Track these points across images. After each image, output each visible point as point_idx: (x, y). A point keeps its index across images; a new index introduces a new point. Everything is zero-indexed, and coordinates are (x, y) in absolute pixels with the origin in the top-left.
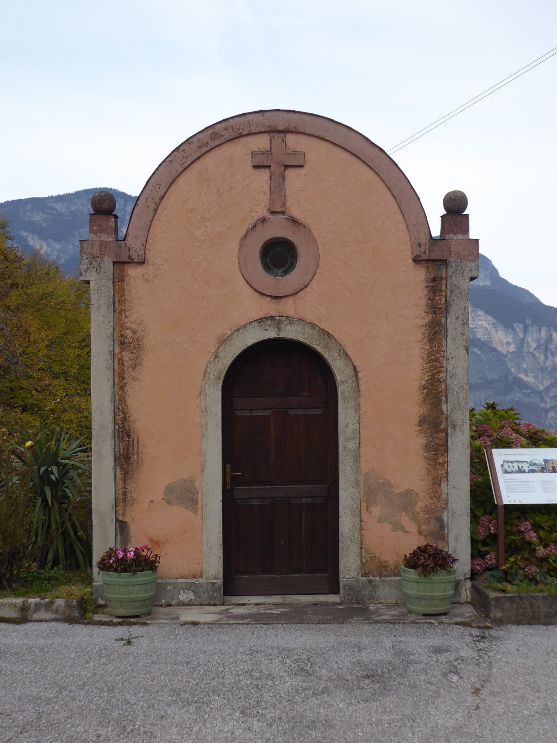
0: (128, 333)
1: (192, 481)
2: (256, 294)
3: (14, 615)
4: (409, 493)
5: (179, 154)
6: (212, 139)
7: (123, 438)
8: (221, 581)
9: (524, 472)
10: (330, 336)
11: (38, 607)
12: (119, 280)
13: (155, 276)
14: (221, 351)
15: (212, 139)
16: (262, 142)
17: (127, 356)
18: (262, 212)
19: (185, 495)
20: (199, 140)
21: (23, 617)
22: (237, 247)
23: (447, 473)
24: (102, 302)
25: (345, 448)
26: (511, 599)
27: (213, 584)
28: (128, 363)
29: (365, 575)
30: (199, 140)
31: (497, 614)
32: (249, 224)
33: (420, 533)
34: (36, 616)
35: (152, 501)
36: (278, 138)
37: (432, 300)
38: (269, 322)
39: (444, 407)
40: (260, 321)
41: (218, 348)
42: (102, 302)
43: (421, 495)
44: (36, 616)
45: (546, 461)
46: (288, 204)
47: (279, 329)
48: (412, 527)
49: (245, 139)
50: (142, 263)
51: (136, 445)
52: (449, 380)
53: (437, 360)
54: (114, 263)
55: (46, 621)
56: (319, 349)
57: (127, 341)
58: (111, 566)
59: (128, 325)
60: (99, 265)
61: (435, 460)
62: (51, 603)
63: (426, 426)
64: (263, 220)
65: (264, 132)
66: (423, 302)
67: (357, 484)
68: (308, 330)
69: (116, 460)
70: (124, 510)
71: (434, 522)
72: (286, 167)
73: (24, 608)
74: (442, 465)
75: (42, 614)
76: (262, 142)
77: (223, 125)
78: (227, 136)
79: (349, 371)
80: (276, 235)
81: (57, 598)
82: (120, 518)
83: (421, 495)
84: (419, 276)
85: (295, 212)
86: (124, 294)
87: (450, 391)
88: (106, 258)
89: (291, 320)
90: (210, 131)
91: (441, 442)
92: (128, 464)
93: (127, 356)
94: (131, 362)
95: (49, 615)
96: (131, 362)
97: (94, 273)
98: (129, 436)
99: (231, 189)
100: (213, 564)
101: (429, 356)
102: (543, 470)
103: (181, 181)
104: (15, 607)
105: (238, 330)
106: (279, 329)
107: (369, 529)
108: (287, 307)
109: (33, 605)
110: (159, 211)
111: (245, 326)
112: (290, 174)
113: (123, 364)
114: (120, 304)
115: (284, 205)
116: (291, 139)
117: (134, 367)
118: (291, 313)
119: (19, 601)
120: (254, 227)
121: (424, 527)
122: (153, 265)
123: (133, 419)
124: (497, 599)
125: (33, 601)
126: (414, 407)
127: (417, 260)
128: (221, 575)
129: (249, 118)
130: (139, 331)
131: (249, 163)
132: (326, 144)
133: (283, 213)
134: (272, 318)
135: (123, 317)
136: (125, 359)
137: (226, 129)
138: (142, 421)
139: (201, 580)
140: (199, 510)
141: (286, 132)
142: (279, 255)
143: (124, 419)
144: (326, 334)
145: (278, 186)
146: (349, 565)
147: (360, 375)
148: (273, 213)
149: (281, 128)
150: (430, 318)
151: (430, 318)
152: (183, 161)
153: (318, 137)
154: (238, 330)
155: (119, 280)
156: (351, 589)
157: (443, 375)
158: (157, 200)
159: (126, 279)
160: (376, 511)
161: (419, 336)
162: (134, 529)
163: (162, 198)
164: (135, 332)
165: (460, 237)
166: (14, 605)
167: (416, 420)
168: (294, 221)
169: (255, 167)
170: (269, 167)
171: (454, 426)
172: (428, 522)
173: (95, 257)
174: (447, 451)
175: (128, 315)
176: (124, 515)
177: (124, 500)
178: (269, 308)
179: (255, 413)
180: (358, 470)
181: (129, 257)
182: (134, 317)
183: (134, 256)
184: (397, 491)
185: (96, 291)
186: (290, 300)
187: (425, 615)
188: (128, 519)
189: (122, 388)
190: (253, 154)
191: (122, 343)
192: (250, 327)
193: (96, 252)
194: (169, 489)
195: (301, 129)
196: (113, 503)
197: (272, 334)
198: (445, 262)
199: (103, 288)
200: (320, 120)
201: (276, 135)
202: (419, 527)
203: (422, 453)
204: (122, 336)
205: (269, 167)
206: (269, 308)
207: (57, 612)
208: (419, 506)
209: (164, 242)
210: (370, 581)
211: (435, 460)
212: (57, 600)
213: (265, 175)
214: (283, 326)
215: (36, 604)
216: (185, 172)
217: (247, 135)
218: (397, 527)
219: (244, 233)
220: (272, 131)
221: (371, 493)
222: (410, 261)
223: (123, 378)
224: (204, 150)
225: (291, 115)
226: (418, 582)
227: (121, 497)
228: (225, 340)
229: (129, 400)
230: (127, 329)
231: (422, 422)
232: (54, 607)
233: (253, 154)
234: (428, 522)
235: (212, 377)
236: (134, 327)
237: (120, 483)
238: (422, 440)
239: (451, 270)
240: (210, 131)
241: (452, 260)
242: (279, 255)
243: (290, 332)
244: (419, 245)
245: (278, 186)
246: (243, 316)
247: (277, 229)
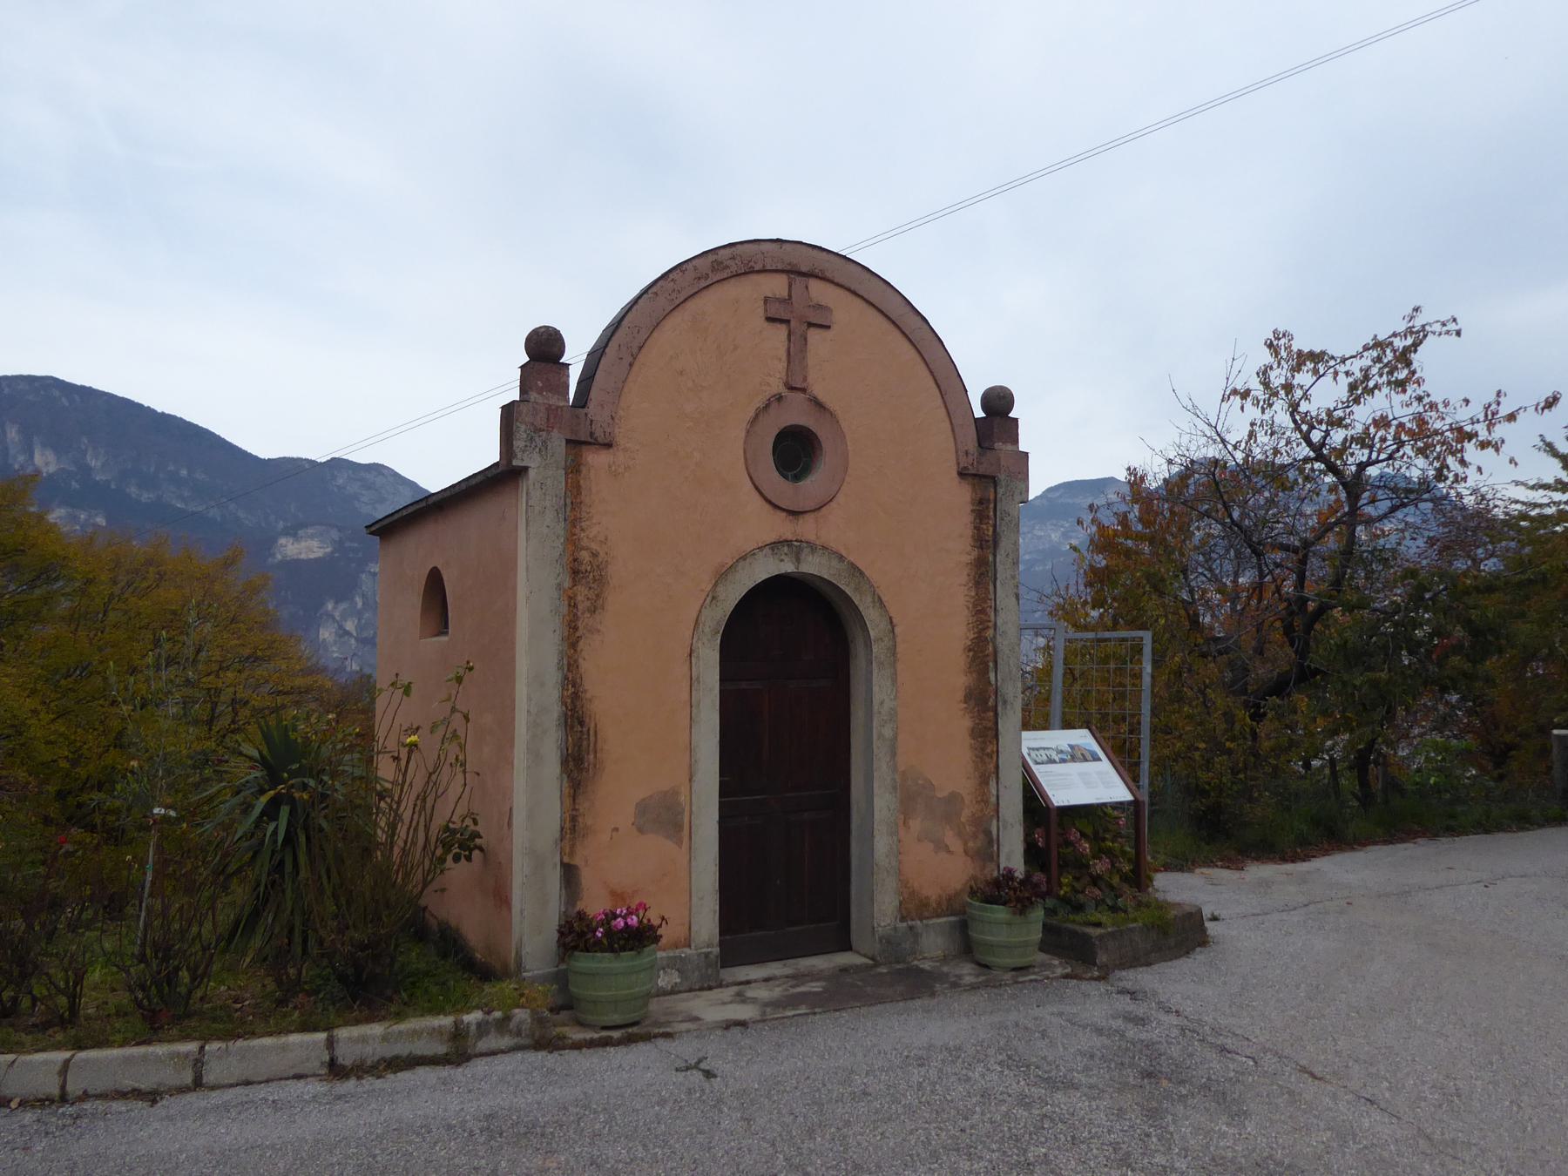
0: (585, 555)
1: (675, 793)
2: (767, 506)
3: (441, 1049)
4: (954, 798)
5: (669, 285)
6: (714, 270)
7: (572, 727)
8: (716, 950)
9: (1054, 762)
10: (861, 573)
11: (483, 1030)
12: (574, 469)
13: (627, 468)
14: (720, 589)
15: (714, 270)
16: (776, 285)
17: (582, 592)
18: (777, 386)
19: (665, 816)
20: (696, 268)
21: (458, 1052)
22: (743, 434)
23: (997, 767)
24: (548, 504)
25: (880, 736)
26: (1112, 935)
27: (707, 955)
28: (583, 606)
29: (903, 919)
30: (696, 268)
31: (1102, 958)
32: (759, 402)
33: (966, 852)
34: (482, 1045)
35: (616, 829)
36: (799, 282)
37: (977, 528)
38: (786, 549)
39: (992, 676)
40: (775, 546)
41: (715, 585)
42: (548, 504)
43: (967, 799)
44: (482, 1045)
45: (1072, 747)
46: (810, 379)
47: (798, 560)
48: (955, 844)
49: (755, 277)
50: (609, 446)
51: (592, 738)
52: (999, 639)
53: (983, 611)
54: (568, 442)
55: (503, 1052)
56: (848, 591)
57: (583, 568)
58: (598, 942)
59: (585, 543)
60: (544, 442)
61: (983, 749)
62: (507, 1018)
63: (972, 703)
64: (780, 398)
65: (782, 271)
66: (969, 532)
67: (895, 788)
68: (835, 563)
69: (564, 762)
70: (573, 847)
71: (981, 836)
72: (810, 325)
73: (458, 1034)
74: (990, 756)
75: (492, 1041)
76: (776, 285)
77: (728, 251)
78: (734, 269)
79: (884, 625)
80: (801, 423)
81: (518, 1007)
82: (566, 860)
83: (967, 799)
84: (962, 496)
85: (818, 391)
86: (579, 493)
87: (1000, 655)
88: (555, 434)
89: (813, 547)
90: (711, 258)
91: (990, 725)
92: (580, 770)
93: (582, 592)
94: (588, 604)
95: (506, 1041)
96: (588, 604)
97: (536, 455)
98: (582, 723)
99: (736, 348)
100: (706, 923)
101: (975, 605)
102: (1073, 759)
103: (668, 324)
104: (441, 1034)
105: (744, 558)
106: (798, 560)
107: (904, 851)
108: (807, 529)
109: (473, 1028)
110: (635, 368)
111: (752, 554)
112: (814, 336)
113: (575, 606)
114: (573, 509)
115: (805, 379)
116: (816, 287)
117: (593, 610)
118: (812, 537)
119: (446, 1021)
120: (767, 406)
121: (971, 844)
122: (625, 450)
123: (588, 695)
124: (1101, 937)
125: (473, 1017)
126: (959, 679)
127: (962, 474)
128: (717, 939)
129: (764, 247)
130: (602, 554)
131: (761, 311)
132: (859, 301)
133: (803, 390)
134: (788, 543)
135: (577, 531)
136: (579, 598)
137: (733, 258)
138: (603, 699)
139: (687, 950)
140: (686, 839)
141: (810, 275)
142: (796, 451)
143: (576, 696)
144: (855, 570)
145: (796, 353)
146: (878, 906)
147: (897, 630)
148: (792, 389)
149: (804, 269)
150: (975, 553)
151: (975, 553)
152: (674, 296)
153: (849, 290)
154: (744, 558)
155: (574, 469)
156: (889, 942)
157: (990, 632)
158: (635, 351)
159: (584, 470)
160: (916, 824)
161: (964, 578)
162: (587, 878)
163: (640, 348)
164: (595, 555)
165: (1010, 447)
166: (436, 1032)
167: (960, 695)
168: (818, 404)
169: (770, 319)
170: (787, 322)
171: (1005, 702)
172: (975, 836)
173: (538, 430)
174: (996, 736)
175: (1415, 404)
176: (572, 854)
177: (573, 829)
178: (782, 528)
179: (744, 685)
180: (895, 769)
181: (592, 434)
182: (593, 532)
183: (599, 433)
184: (940, 795)
185: (538, 486)
186: (809, 518)
187: (1014, 969)
188: (577, 861)
189: (574, 645)
190: (766, 300)
191: (575, 572)
192: (760, 555)
193: (540, 421)
194: (642, 808)
195: (828, 275)
196: (558, 835)
197: (788, 567)
198: (993, 480)
199: (549, 482)
200: (852, 266)
201: (798, 279)
202: (965, 844)
203: (969, 741)
204: (575, 560)
205: (787, 322)
206: (782, 528)
207: (519, 1034)
208: (965, 815)
209: (639, 414)
210: (911, 928)
211: (983, 749)
212: (517, 1011)
213: (782, 331)
214: (803, 556)
215: (479, 1025)
216: (675, 313)
217: (759, 272)
218: (941, 846)
219: (752, 414)
220: (793, 272)
221: (911, 797)
222: (955, 474)
223: (576, 629)
224: (703, 284)
225: (815, 252)
226: (1009, 924)
227: (568, 825)
228: (726, 573)
229: (584, 665)
230: (583, 548)
231: (968, 697)
232: (512, 1025)
233: (766, 300)
234: (975, 836)
235: (707, 630)
236: (594, 546)
237: (568, 802)
238: (967, 723)
239: (1000, 491)
240: (711, 258)
241: (1002, 477)
242: (796, 451)
243: (813, 566)
244: (967, 453)
245: (796, 353)
246: (746, 537)
247: (796, 414)
